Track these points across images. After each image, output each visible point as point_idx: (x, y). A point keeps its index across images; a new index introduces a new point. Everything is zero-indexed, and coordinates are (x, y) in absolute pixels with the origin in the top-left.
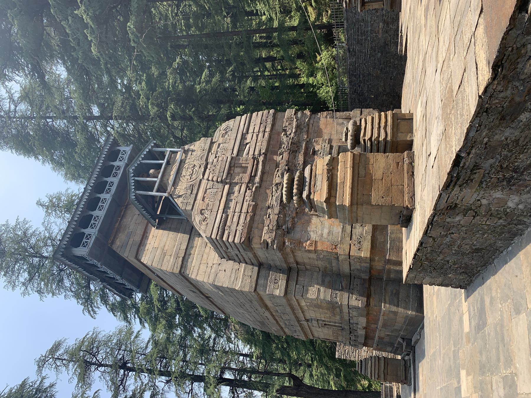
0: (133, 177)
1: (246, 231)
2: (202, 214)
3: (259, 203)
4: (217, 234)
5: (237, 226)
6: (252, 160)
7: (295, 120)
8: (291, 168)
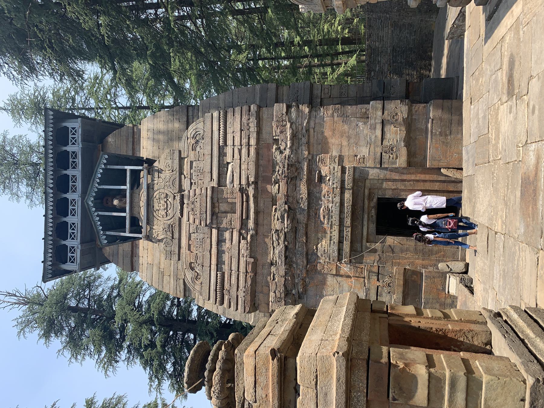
0: (95, 211)
1: (249, 298)
2: (192, 269)
3: (259, 257)
4: (216, 299)
5: (238, 290)
6: (239, 194)
7: (288, 125)
8: (292, 207)
